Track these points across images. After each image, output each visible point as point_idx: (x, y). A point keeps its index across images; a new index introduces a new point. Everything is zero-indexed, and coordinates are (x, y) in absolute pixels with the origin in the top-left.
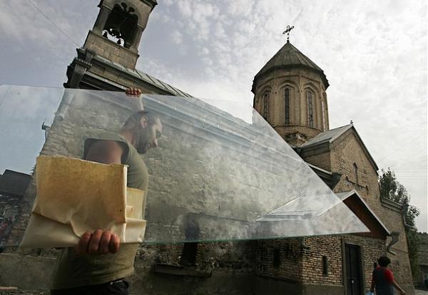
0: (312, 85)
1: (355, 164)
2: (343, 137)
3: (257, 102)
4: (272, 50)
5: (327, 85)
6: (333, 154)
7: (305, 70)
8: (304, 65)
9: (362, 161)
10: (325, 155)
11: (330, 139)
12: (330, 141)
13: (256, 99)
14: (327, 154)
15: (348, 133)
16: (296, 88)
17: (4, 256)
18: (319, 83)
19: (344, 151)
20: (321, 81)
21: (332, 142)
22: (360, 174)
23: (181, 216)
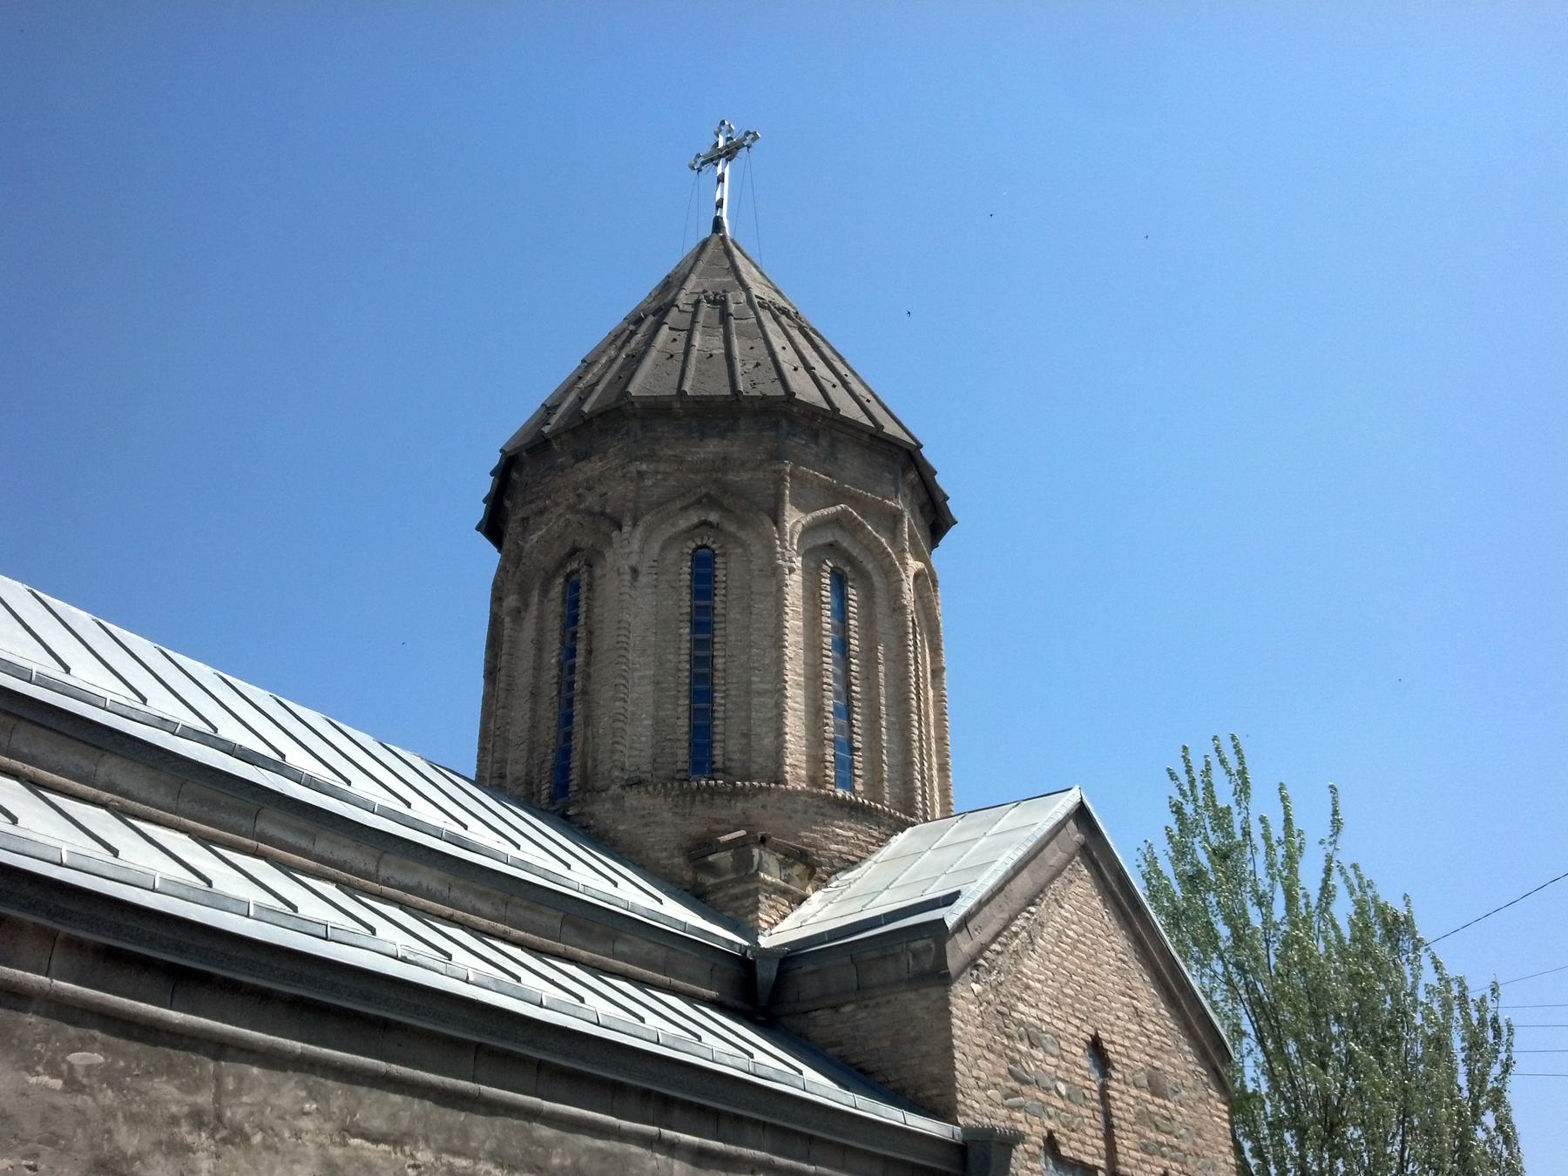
0: (854, 529)
1: (1096, 1047)
2: (1024, 883)
3: (517, 614)
4: (949, 495)
5: (937, 520)
6: (966, 1000)
7: (815, 436)
8: (810, 410)
9: (1138, 1013)
10: (916, 1003)
11: (950, 899)
12: (951, 915)
13: (289, 775)
14: (935, 993)
15: (1054, 856)
16: (756, 548)
17: (804, 397)
18: (896, 517)
19: (1030, 965)
20: (898, 504)
21: (963, 923)
22: (1125, 1100)
23: (231, 1088)
